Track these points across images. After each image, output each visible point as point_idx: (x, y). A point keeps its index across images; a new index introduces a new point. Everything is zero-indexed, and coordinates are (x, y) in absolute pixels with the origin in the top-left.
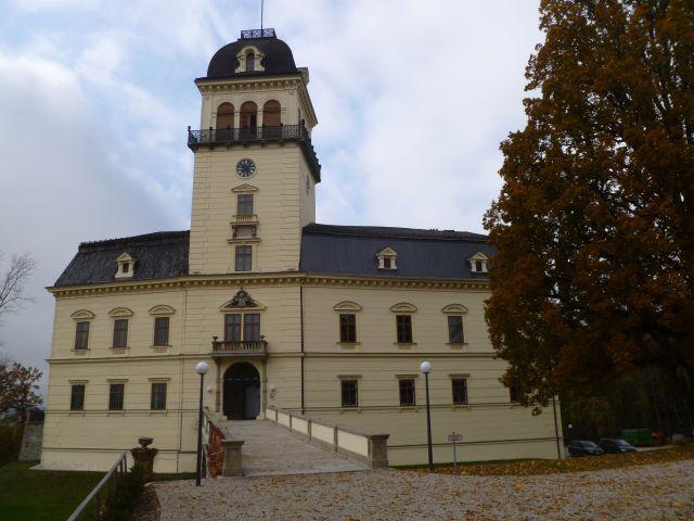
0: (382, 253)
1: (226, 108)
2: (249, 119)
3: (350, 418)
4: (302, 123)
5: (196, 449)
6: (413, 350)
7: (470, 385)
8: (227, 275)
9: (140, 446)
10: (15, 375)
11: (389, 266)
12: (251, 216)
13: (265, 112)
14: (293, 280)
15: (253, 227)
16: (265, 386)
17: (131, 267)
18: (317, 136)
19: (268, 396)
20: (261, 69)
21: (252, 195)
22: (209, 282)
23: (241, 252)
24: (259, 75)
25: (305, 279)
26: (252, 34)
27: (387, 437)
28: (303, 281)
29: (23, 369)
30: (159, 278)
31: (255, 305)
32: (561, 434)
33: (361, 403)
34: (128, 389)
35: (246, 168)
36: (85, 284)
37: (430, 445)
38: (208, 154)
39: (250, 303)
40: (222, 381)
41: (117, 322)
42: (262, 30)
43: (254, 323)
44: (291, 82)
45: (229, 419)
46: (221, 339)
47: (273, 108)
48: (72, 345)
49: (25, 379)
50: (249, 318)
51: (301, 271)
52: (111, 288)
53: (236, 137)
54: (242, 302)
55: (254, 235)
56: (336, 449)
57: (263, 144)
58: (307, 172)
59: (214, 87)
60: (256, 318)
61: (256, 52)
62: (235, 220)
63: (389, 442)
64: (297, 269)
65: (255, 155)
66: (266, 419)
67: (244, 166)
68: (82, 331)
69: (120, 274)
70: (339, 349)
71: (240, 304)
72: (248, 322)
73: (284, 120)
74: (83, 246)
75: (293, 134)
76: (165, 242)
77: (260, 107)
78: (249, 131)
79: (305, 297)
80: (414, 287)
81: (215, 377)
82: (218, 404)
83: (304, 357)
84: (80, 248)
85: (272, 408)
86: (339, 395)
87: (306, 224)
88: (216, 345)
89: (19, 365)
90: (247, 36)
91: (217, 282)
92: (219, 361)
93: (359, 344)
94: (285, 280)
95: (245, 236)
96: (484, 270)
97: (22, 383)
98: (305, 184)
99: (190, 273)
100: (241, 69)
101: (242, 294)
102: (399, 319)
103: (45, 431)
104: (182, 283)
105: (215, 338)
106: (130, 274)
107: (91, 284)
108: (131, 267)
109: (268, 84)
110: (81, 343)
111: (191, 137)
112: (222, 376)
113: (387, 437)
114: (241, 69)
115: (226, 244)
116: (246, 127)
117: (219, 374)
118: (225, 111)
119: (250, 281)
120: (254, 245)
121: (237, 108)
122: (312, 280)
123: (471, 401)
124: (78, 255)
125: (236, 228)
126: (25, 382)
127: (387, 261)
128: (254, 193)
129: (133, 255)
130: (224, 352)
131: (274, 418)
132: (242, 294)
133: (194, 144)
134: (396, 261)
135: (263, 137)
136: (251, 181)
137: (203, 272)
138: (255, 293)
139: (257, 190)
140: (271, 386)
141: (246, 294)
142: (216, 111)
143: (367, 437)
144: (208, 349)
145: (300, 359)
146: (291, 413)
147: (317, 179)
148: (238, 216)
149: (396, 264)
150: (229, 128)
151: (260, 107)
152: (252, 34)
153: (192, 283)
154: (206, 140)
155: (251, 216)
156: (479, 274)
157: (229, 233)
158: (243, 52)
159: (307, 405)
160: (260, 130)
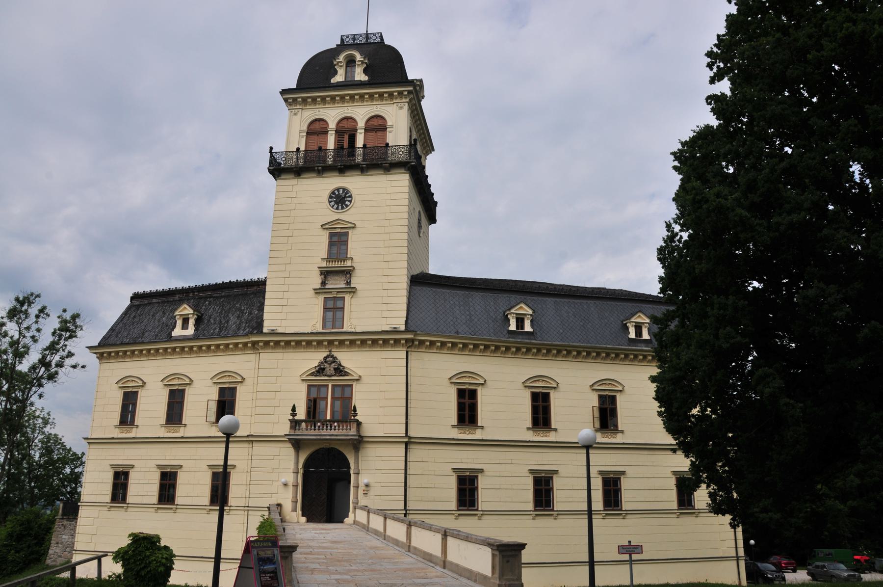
0: (513, 311)
1: (317, 126)
2: (346, 137)
3: (467, 524)
4: (412, 145)
5: (633, 565)
6: (551, 437)
7: (483, 483)
8: (312, 334)
10: (64, 461)
11: (523, 328)
12: (346, 258)
13: (367, 130)
14: (397, 341)
15: (347, 273)
16: (357, 480)
17: (192, 322)
18: (432, 166)
20: (364, 78)
21: (347, 234)
22: (288, 343)
23: (330, 304)
24: (361, 84)
25: (413, 340)
26: (354, 39)
27: (522, 546)
28: (410, 345)
29: (75, 454)
30: (226, 337)
31: (347, 374)
32: (741, 552)
33: (482, 506)
34: (557, 483)
35: (340, 199)
36: (135, 343)
37: (592, 563)
38: (294, 182)
39: (340, 371)
40: (301, 471)
41: (171, 392)
42: (367, 34)
43: (344, 397)
44: (400, 93)
45: (308, 521)
47: (377, 125)
48: (117, 421)
49: (76, 467)
50: (339, 390)
51: (407, 331)
52: (166, 349)
53: (330, 161)
54: (330, 369)
55: (348, 283)
56: (445, 564)
57: (364, 169)
58: (418, 207)
59: (304, 100)
60: (347, 390)
61: (359, 57)
62: (324, 264)
63: (526, 556)
64: (403, 328)
65: (353, 182)
66: (355, 522)
67: (338, 196)
68: (130, 401)
69: (177, 332)
70: (455, 434)
72: (337, 395)
73: (391, 139)
74: (136, 297)
75: (402, 156)
77: (361, 124)
78: (345, 152)
80: (622, 360)
81: (291, 465)
83: (408, 442)
84: (132, 298)
85: (364, 508)
86: (530, 495)
87: (416, 272)
88: (295, 424)
89: (70, 450)
90: (348, 41)
91: (298, 343)
92: (297, 445)
93: (622, 432)
94: (386, 342)
95: (336, 283)
96: (646, 336)
97: (72, 472)
98: (416, 221)
99: (265, 330)
100: (339, 78)
101: (330, 359)
102: (461, 393)
103: (79, 529)
104: (254, 344)
106: (191, 331)
107: (143, 343)
108: (192, 322)
109: (371, 96)
110: (127, 416)
111: (273, 161)
112: (301, 465)
113: (522, 546)
114: (339, 78)
115: (299, 379)
116: (342, 148)
117: (297, 463)
118: (316, 129)
119: (342, 343)
120: (347, 297)
121: (332, 125)
122: (422, 343)
123: (625, 506)
124: (129, 309)
125: (326, 274)
126: (76, 470)
127: (520, 321)
128: (350, 232)
129: (195, 309)
130: (307, 433)
131: (365, 522)
132: (330, 359)
133: (277, 169)
134: (532, 321)
135: (364, 160)
136: (348, 216)
137: (280, 330)
138: (347, 359)
140: (363, 479)
141: (335, 358)
142: (305, 128)
143: (490, 545)
144: (284, 428)
145: (403, 446)
146: (385, 515)
147: (432, 219)
148: (328, 259)
149: (532, 326)
150: (320, 149)
151: (361, 124)
152: (354, 39)
154: (292, 163)
155: (346, 258)
156: (639, 340)
157: (317, 282)
158: (341, 58)
159: (411, 506)
160: (359, 151)
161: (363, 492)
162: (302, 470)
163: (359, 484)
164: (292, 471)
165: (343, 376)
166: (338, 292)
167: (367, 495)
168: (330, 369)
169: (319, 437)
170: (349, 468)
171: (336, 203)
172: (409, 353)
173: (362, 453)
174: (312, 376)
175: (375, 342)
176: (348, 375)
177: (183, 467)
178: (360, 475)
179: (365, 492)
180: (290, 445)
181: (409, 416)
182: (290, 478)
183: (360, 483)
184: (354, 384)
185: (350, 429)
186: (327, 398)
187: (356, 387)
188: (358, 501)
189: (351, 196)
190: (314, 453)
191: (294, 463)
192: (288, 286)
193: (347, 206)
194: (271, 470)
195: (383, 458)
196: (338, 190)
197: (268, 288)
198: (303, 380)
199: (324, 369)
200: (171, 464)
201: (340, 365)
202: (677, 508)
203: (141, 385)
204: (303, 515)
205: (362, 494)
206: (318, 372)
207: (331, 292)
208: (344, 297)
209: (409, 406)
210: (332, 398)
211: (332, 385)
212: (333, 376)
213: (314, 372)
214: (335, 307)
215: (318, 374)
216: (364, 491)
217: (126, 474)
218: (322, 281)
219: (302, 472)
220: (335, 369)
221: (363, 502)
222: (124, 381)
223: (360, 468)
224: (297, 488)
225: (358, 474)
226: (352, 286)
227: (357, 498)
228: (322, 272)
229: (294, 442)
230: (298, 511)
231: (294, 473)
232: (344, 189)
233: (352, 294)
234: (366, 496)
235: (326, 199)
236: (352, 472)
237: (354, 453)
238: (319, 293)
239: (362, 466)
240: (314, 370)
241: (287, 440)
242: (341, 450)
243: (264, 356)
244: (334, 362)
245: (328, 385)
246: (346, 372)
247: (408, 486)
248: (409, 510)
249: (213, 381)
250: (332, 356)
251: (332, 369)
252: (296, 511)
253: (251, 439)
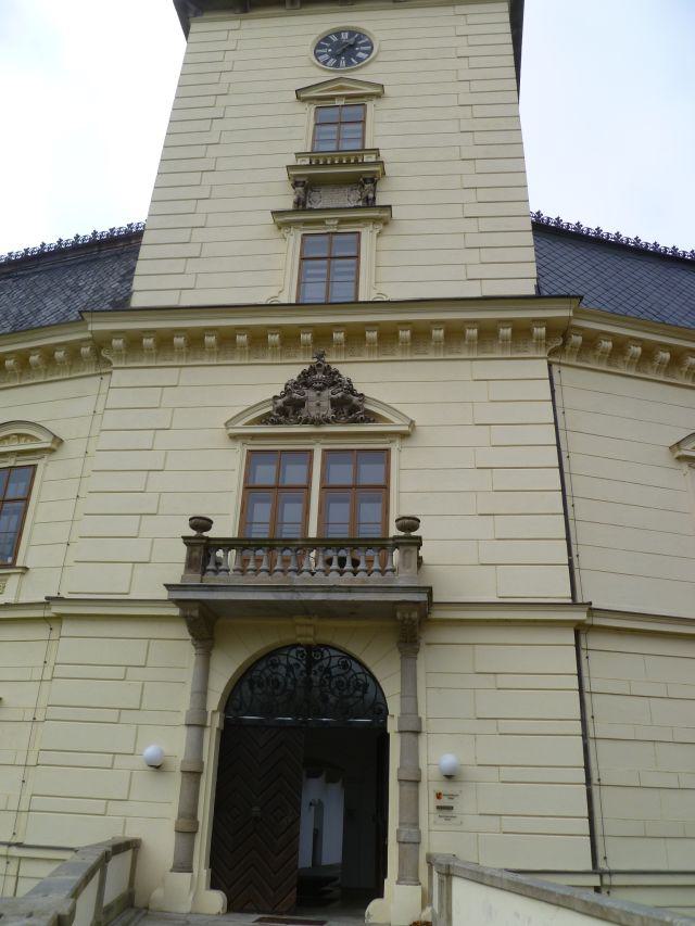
9: (193, 533)
14: (522, 332)
16: (412, 753)
19: (427, 803)
28: (562, 344)
31: (371, 417)
35: (345, 49)
39: (350, 407)
40: (215, 722)
45: (233, 906)
46: (225, 526)
54: (319, 402)
55: (369, 203)
71: (311, 410)
76: (70, 257)
79: (566, 398)
81: (184, 702)
82: (187, 831)
88: (202, 547)
101: (319, 377)
104: (100, 344)
105: (200, 524)
112: (214, 701)
115: (221, 435)
117: (202, 692)
119: (355, 338)
122: (591, 342)
130: (236, 580)
132: (319, 377)
138: (369, 377)
139: (378, 94)
140: (438, 755)
153: (134, 343)
161: (434, 802)
164: (182, 719)
165: (362, 421)
166: (342, 221)
168: (319, 402)
169: (285, 596)
170: (380, 711)
171: (338, 57)
172: (555, 368)
173: (426, 660)
175: (455, 335)
176: (374, 421)
178: (422, 739)
179: (445, 802)
180: (182, 631)
182: (173, 743)
183: (423, 765)
184: (395, 447)
186: (308, 488)
187: (400, 457)
188: (419, 833)
189: (370, 44)
190: (258, 662)
191: (193, 693)
192: (194, 276)
193: (360, 60)
194: (112, 715)
196: (338, 34)
197: (144, 252)
198: (234, 437)
199: (300, 404)
201: (351, 391)
204: (214, 885)
205: (433, 808)
206: (282, 411)
207: (321, 222)
208: (359, 233)
210: (323, 488)
211: (325, 451)
212: (328, 421)
213: (269, 414)
214: (280, 484)
215: (282, 418)
216: (439, 796)
218: (299, 199)
220: (334, 403)
221: (437, 839)
223: (422, 714)
224: (197, 783)
226: (380, 201)
227: (416, 824)
228: (298, 179)
229: (196, 613)
230: (195, 869)
231: (188, 725)
232: (352, 33)
233: (380, 227)
234: (447, 818)
235: (309, 50)
236: (392, 726)
237: (399, 656)
238: (288, 224)
239: (430, 705)
240: (270, 409)
242: (354, 649)
243: (121, 378)
244: (334, 384)
245: (311, 451)
246: (367, 412)
247: (595, 781)
248: (610, 873)
250: (327, 370)
251: (326, 404)
252: (192, 872)
253: (56, 609)
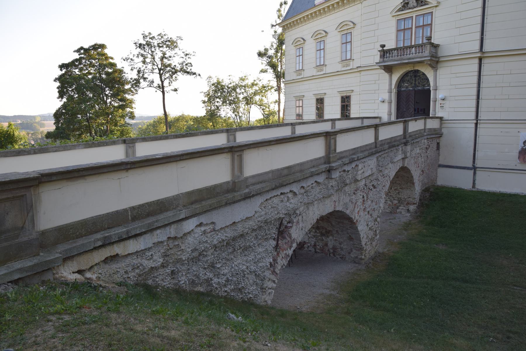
16: (435, 94)
117: (391, 84)
161: (440, 105)
162: (394, 90)
163: (436, 99)
165: (424, 5)
167: (444, 108)
170: (429, 85)
174: (400, 11)
177: (305, 96)
178: (437, 91)
179: (442, 105)
181: (484, 33)
182: (386, 96)
183: (437, 97)
185: (425, 52)
191: (389, 85)
195: (458, 75)
200: (347, 90)
202: (295, 119)
203: (352, 26)
205: (439, 107)
206: (403, 6)
209: (485, 22)
212: (415, 7)
213: (400, 8)
216: (441, 104)
217: (348, 97)
219: (394, 92)
222: (316, 34)
223: (438, 85)
225: (436, 90)
240: (400, 6)
241: (378, 67)
248: (480, 120)
249: (392, 15)
